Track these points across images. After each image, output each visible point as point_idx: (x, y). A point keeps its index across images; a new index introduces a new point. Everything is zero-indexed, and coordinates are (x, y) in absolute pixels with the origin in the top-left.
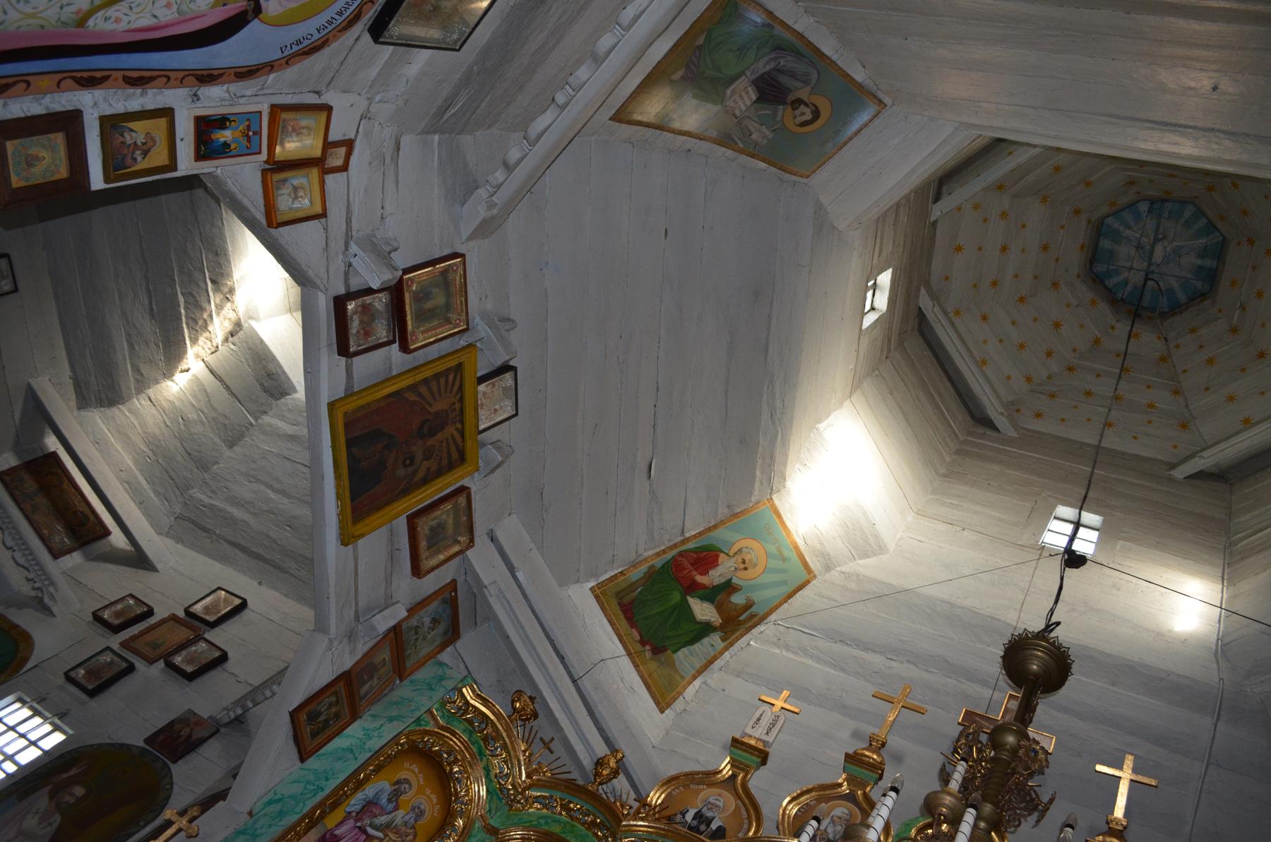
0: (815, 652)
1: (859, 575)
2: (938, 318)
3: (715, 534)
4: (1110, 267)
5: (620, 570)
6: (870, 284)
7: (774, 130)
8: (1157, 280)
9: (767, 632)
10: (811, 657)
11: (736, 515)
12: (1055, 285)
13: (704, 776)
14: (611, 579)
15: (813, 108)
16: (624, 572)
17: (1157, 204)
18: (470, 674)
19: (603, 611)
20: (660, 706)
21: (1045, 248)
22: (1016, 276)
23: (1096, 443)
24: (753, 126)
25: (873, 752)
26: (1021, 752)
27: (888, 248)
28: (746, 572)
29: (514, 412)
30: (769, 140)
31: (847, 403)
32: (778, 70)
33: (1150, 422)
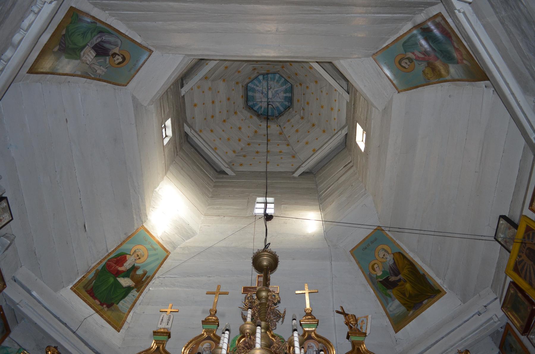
1: (188, 247)
2: (193, 135)
3: (122, 247)
4: (254, 102)
5: (82, 276)
6: (163, 126)
7: (106, 68)
8: (272, 104)
9: (156, 282)
11: (129, 237)
12: (236, 113)
13: (145, 352)
14: (79, 282)
15: (122, 56)
16: (85, 276)
17: (265, 75)
18: (21, 347)
19: (79, 297)
20: (117, 329)
21: (229, 99)
22: (220, 112)
23: (265, 170)
24: (96, 67)
25: (213, 317)
26: (269, 298)
27: (167, 110)
28: (139, 260)
29: (11, 218)
30: (105, 72)
31: (165, 177)
32: (102, 41)
33: (281, 158)
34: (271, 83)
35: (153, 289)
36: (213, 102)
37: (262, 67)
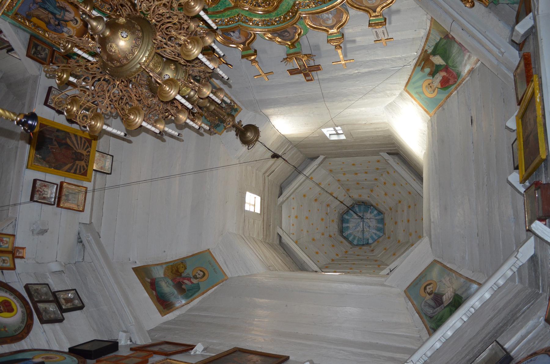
10: (388, 60)
12: (391, 209)
21: (396, 223)
34: (361, 236)
36: (408, 221)
37: (365, 252)
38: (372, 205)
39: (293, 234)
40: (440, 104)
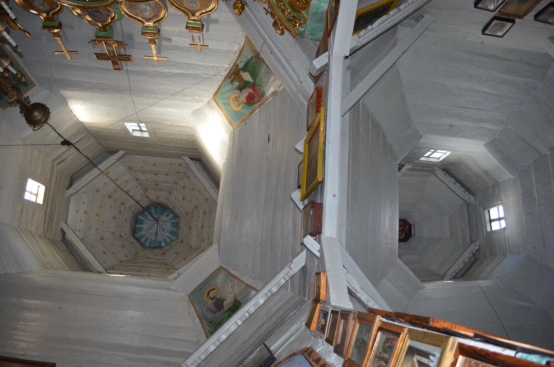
0: (201, 68)
10: (201, 66)
12: (187, 214)
21: (190, 228)
34: (154, 239)
35: (225, 65)
36: (202, 227)
37: (156, 255)
38: (169, 208)
39: (80, 231)
40: (243, 118)
